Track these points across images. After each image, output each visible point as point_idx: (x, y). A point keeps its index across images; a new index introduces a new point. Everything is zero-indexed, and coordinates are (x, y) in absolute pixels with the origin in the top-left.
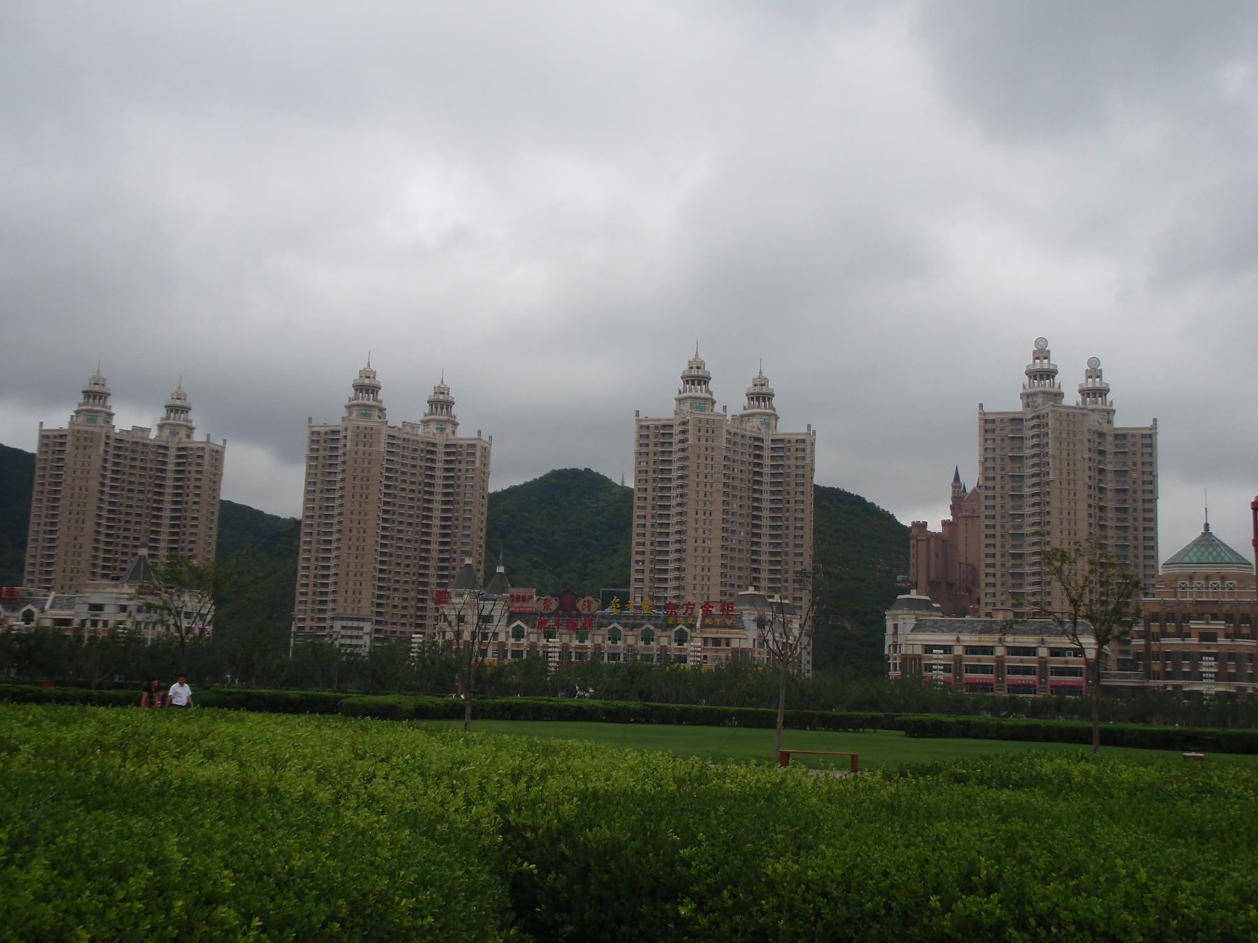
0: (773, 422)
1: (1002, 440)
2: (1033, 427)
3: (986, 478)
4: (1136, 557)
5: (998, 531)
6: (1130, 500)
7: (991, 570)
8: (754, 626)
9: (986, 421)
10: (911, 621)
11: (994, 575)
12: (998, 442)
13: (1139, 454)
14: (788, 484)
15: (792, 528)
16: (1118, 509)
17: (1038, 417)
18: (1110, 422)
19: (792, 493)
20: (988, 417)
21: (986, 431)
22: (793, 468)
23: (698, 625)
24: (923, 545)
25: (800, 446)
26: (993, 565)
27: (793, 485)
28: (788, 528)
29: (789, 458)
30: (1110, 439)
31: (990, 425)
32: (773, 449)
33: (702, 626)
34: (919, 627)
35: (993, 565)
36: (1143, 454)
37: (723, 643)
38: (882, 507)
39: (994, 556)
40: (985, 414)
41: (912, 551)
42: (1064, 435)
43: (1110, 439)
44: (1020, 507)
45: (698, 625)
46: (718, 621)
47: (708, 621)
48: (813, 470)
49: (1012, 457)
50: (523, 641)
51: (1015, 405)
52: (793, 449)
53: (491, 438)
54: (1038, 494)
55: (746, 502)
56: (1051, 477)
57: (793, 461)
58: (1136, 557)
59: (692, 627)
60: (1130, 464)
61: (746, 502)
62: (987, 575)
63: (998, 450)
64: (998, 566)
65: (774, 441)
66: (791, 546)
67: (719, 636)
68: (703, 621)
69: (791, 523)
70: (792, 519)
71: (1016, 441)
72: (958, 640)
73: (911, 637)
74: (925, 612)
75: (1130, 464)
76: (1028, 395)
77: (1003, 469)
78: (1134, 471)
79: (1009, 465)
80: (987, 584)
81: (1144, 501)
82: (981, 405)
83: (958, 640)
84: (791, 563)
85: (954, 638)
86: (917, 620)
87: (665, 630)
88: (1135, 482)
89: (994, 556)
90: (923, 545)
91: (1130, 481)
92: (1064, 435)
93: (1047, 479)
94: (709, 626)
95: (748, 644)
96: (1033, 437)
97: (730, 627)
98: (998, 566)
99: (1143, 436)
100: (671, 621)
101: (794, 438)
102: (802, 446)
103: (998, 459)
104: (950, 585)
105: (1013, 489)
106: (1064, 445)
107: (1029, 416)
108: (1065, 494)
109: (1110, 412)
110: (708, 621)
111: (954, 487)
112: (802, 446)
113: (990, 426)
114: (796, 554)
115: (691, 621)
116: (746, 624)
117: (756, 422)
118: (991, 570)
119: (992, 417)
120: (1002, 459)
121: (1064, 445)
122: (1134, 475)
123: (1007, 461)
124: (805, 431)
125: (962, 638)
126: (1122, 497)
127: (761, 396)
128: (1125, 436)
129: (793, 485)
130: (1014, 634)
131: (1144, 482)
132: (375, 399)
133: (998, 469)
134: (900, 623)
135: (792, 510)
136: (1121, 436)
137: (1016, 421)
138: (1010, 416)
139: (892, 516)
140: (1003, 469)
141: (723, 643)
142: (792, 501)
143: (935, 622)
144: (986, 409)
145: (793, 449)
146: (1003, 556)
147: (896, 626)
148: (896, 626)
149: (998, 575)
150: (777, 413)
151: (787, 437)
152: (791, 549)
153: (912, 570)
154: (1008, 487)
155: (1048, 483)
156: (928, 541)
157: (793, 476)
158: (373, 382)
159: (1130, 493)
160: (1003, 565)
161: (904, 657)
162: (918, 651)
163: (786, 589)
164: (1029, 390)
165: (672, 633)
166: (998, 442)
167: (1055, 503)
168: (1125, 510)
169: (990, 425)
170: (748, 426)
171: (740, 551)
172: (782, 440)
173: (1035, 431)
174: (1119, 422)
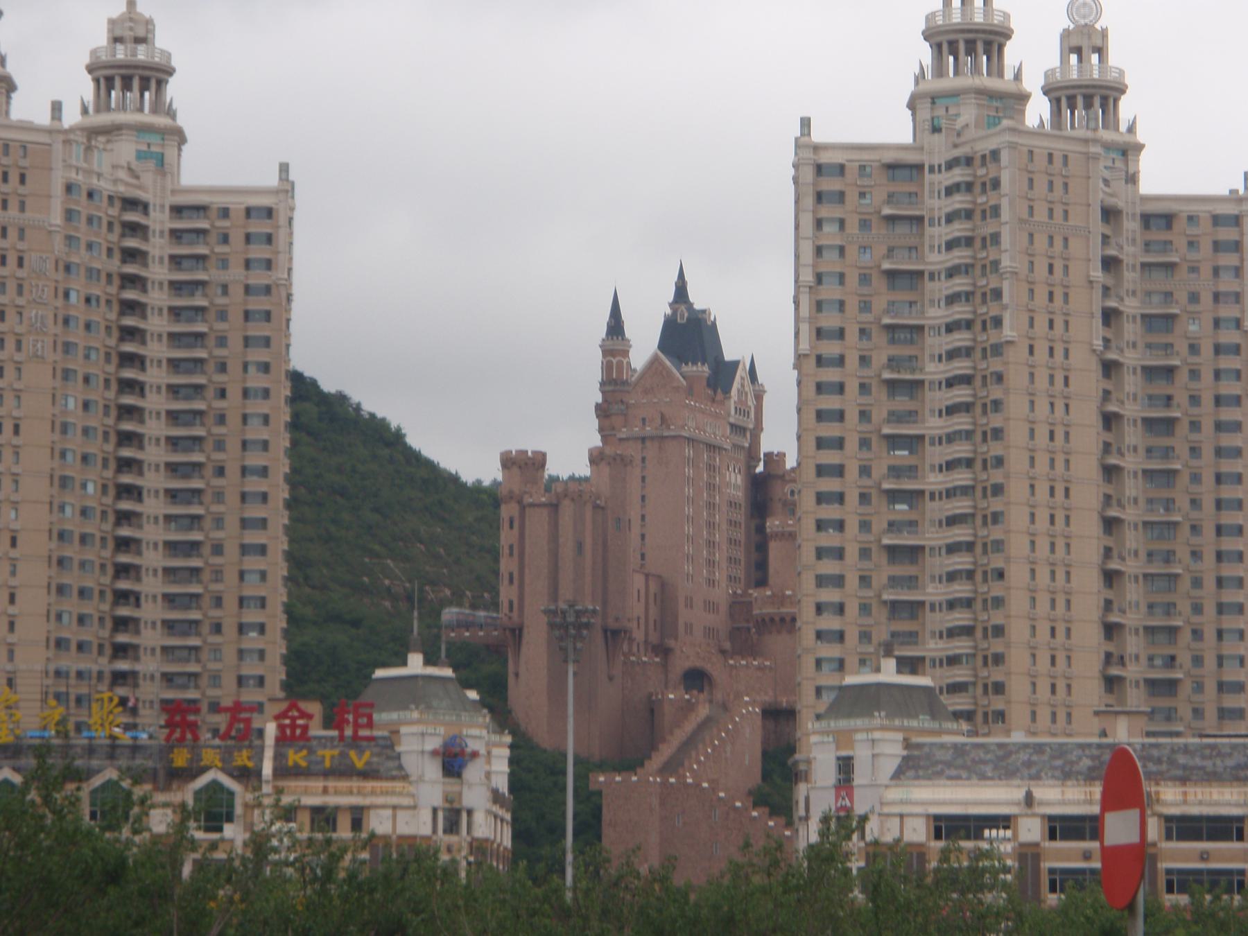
0: (170, 153)
1: (865, 224)
2: (950, 191)
3: (819, 333)
4: (1196, 555)
5: (851, 484)
6: (1181, 398)
7: (830, 595)
8: (433, 770)
9: (819, 169)
10: (892, 748)
11: (840, 609)
12: (853, 227)
13: (1206, 270)
14: (222, 341)
15: (233, 470)
16: (1149, 423)
17: (969, 161)
18: (1132, 179)
19: (234, 367)
20: (825, 158)
21: (819, 197)
22: (237, 292)
23: (267, 769)
24: (538, 523)
25: (259, 227)
26: (839, 581)
27: (235, 342)
28: (220, 471)
29: (224, 263)
30: (1131, 226)
31: (826, 179)
32: (176, 235)
33: (282, 771)
34: (914, 765)
35: (839, 581)
36: (1216, 271)
37: (344, 822)
38: (368, 406)
39: (839, 554)
40: (817, 148)
41: (507, 537)
42: (1041, 215)
43: (1131, 226)
44: (911, 416)
45: (267, 769)
46: (328, 755)
47: (295, 757)
48: (289, 298)
49: (892, 275)
50: (229, 830)
51: (894, 128)
52: (237, 238)
53: (284, 168)
54: (966, 380)
55: (97, 394)
56: (1008, 332)
57: (236, 273)
58: (1196, 555)
59: (249, 775)
60: (1182, 296)
61: (97, 394)
62: (819, 609)
63: (852, 252)
64: (852, 581)
65: (177, 210)
66: (232, 523)
67: (332, 800)
68: (279, 757)
69: (231, 457)
70: (233, 445)
71: (902, 229)
72: (1029, 800)
73: (894, 794)
74: (924, 722)
75: (1182, 296)
76: (934, 98)
77: (865, 306)
78: (1194, 316)
79: (882, 297)
80: (819, 635)
81: (1218, 401)
82: (806, 123)
83: (1029, 800)
84: (231, 577)
85: (1019, 794)
86: (907, 745)
87: (167, 788)
88: (1194, 349)
89: (839, 554)
90: (538, 523)
91: (1182, 347)
92: (1041, 215)
93: (993, 337)
94: (297, 772)
95: (419, 824)
96: (950, 218)
97: (366, 775)
98: (852, 581)
99: (1217, 220)
100: (181, 759)
101: (238, 204)
102: (250, 233)
103: (852, 280)
104: (614, 635)
105: (893, 363)
106: (1041, 242)
107: (940, 158)
108: (1042, 382)
109: (1128, 151)
110: (295, 757)
111: (607, 352)
112: (250, 233)
113: (831, 184)
114: (245, 549)
115: (242, 759)
116: (411, 763)
117: (126, 149)
118: (830, 595)
119: (838, 158)
120: (865, 279)
121: (1041, 242)
122: (1193, 328)
123: (879, 283)
124: (273, 181)
125: (1038, 793)
126: (1161, 388)
127: (130, 74)
128: (1168, 220)
129: (235, 342)
130: (1183, 781)
131: (1218, 349)
132: (159, 106)
133: (852, 305)
134: (861, 754)
135: (234, 420)
136: (1161, 218)
137: (901, 169)
138: (889, 157)
139: (398, 437)
140: (865, 306)
141: (344, 822)
142: (234, 393)
143: (959, 750)
144: (818, 135)
145: (237, 238)
146: (865, 553)
147: (846, 766)
148: (846, 766)
149: (852, 609)
150: (181, 121)
151: (219, 201)
152: (230, 534)
153: (506, 592)
154: (880, 358)
155: (997, 349)
156: (554, 507)
157: (236, 316)
158: (142, 54)
159: (1183, 377)
160: (864, 580)
161: (875, 851)
162: (917, 832)
163: (216, 649)
164: (932, 84)
165: (187, 794)
166: (853, 227)
167: (1016, 406)
168: (1168, 425)
169: (826, 179)
170: (101, 161)
171: (84, 539)
172: (201, 209)
173: (959, 201)
174: (1160, 176)
